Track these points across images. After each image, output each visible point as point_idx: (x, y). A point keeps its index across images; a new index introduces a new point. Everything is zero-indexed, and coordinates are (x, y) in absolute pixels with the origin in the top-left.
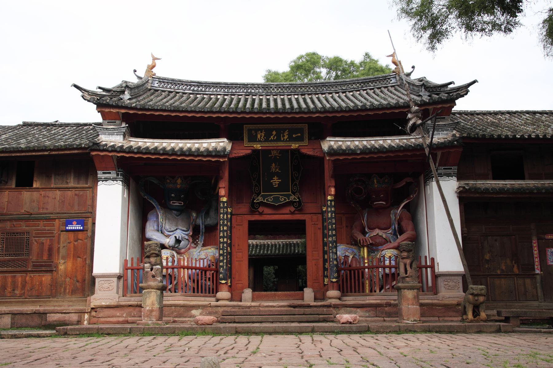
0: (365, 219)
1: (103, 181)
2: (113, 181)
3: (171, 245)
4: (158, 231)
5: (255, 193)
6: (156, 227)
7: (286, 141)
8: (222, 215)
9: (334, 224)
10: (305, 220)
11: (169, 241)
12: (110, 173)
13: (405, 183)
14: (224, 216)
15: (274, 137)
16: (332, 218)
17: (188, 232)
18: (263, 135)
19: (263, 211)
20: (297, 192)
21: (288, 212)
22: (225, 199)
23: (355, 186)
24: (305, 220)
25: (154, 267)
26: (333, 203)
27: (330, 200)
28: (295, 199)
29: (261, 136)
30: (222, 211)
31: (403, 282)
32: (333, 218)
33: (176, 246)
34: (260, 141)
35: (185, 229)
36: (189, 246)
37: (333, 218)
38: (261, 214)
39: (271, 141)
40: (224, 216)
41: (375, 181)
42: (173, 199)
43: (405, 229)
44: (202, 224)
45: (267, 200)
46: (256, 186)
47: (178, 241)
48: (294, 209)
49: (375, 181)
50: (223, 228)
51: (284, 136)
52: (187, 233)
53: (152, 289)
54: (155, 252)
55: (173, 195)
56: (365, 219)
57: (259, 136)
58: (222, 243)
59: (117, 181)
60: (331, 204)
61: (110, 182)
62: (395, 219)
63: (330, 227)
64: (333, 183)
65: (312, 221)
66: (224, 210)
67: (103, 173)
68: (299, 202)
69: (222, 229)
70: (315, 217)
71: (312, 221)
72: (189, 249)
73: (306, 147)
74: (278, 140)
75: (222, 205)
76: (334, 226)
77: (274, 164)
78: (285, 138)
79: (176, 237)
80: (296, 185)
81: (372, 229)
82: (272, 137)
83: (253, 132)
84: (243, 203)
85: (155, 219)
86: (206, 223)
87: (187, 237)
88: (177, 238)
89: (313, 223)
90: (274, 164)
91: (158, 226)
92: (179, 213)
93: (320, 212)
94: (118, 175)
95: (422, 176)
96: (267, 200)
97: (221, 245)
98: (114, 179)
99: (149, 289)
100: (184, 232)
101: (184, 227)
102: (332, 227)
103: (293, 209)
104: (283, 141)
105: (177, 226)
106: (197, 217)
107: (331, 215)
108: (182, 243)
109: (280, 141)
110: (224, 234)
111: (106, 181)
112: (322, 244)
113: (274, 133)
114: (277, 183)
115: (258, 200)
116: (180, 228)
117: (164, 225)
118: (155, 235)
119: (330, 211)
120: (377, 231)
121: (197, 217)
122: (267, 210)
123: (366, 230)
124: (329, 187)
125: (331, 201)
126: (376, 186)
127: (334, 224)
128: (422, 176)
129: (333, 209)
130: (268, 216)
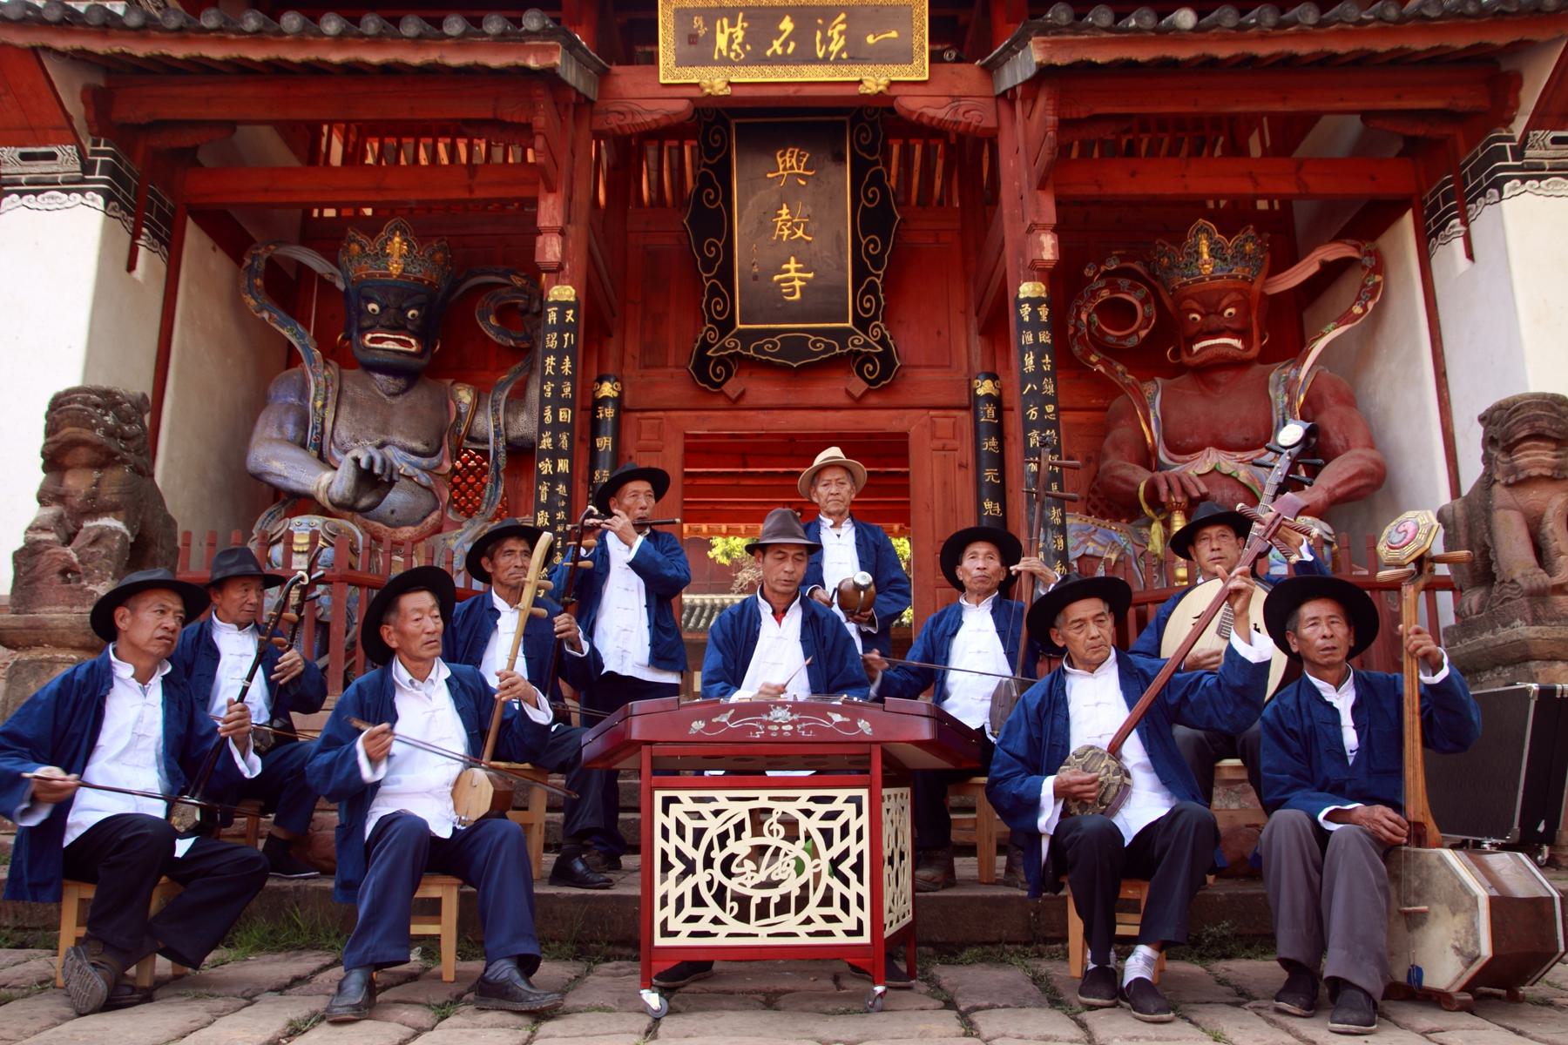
0: (1155, 412)
1: (22, 194)
2: (67, 192)
3: (337, 498)
4: (303, 446)
5: (712, 321)
6: (290, 430)
7: (839, 61)
8: (550, 361)
9: (1049, 400)
10: (905, 435)
11: (332, 482)
12: (52, 156)
13: (1314, 268)
14: (559, 362)
15: (785, 45)
16: (1038, 375)
17: (435, 460)
18: (739, 34)
19: (742, 394)
20: (875, 317)
21: (842, 400)
22: (563, 292)
23: (1105, 294)
24: (905, 435)
25: (88, 524)
26: (1044, 312)
27: (1028, 300)
28: (866, 344)
29: (731, 41)
30: (552, 343)
31: (1536, 620)
32: (1047, 374)
33: (365, 502)
34: (725, 62)
35: (418, 445)
36: (435, 516)
37: (1047, 374)
38: (735, 404)
39: (782, 60)
40: (559, 362)
41: (1205, 249)
42: (376, 323)
43: (1338, 441)
44: (497, 434)
45: (759, 349)
46: (714, 291)
47: (371, 480)
48: (865, 386)
49: (1205, 249)
50: (555, 414)
51: (827, 41)
52: (425, 462)
53: (59, 645)
54: (86, 434)
55: (372, 306)
56: (1155, 412)
57: (721, 41)
58: (548, 477)
59: (82, 192)
60: (1034, 314)
61: (54, 197)
62: (1290, 404)
63: (1033, 413)
64: (1049, 213)
65: (933, 437)
66: (561, 340)
67: (25, 157)
68: (886, 358)
69: (548, 419)
70: (943, 421)
71: (933, 437)
72: (438, 530)
73: (919, 90)
74: (805, 56)
75: (552, 317)
76: (1050, 408)
77: (785, 211)
78: (834, 48)
79: (357, 460)
80: (872, 288)
81: (1182, 448)
82: (777, 45)
83: (698, 22)
84: (665, 366)
85: (293, 400)
86: (513, 434)
87: (424, 479)
88: (363, 464)
89: (938, 443)
90: (785, 211)
91: (303, 423)
92: (401, 382)
93: (966, 402)
94: (88, 167)
95: (1408, 219)
96: (759, 349)
97: (544, 489)
98: (72, 185)
99: (38, 644)
100: (414, 458)
101: (416, 438)
102: (1042, 412)
103: (858, 386)
104: (825, 60)
105: (384, 430)
106: (477, 407)
107: (1038, 362)
108: (396, 498)
109: (815, 61)
110: (556, 442)
111: (36, 193)
112: (1021, 427)
113: (787, 25)
114: (798, 283)
115: (724, 348)
116: (398, 439)
117: (328, 425)
118: (277, 458)
119: (1031, 347)
120: (1210, 460)
121: (477, 407)
122: (762, 390)
123: (1162, 456)
124: (1030, 231)
125: (1034, 302)
126: (1208, 268)
127: (1049, 400)
128: (1408, 219)
129: (1044, 337)
130: (761, 415)
